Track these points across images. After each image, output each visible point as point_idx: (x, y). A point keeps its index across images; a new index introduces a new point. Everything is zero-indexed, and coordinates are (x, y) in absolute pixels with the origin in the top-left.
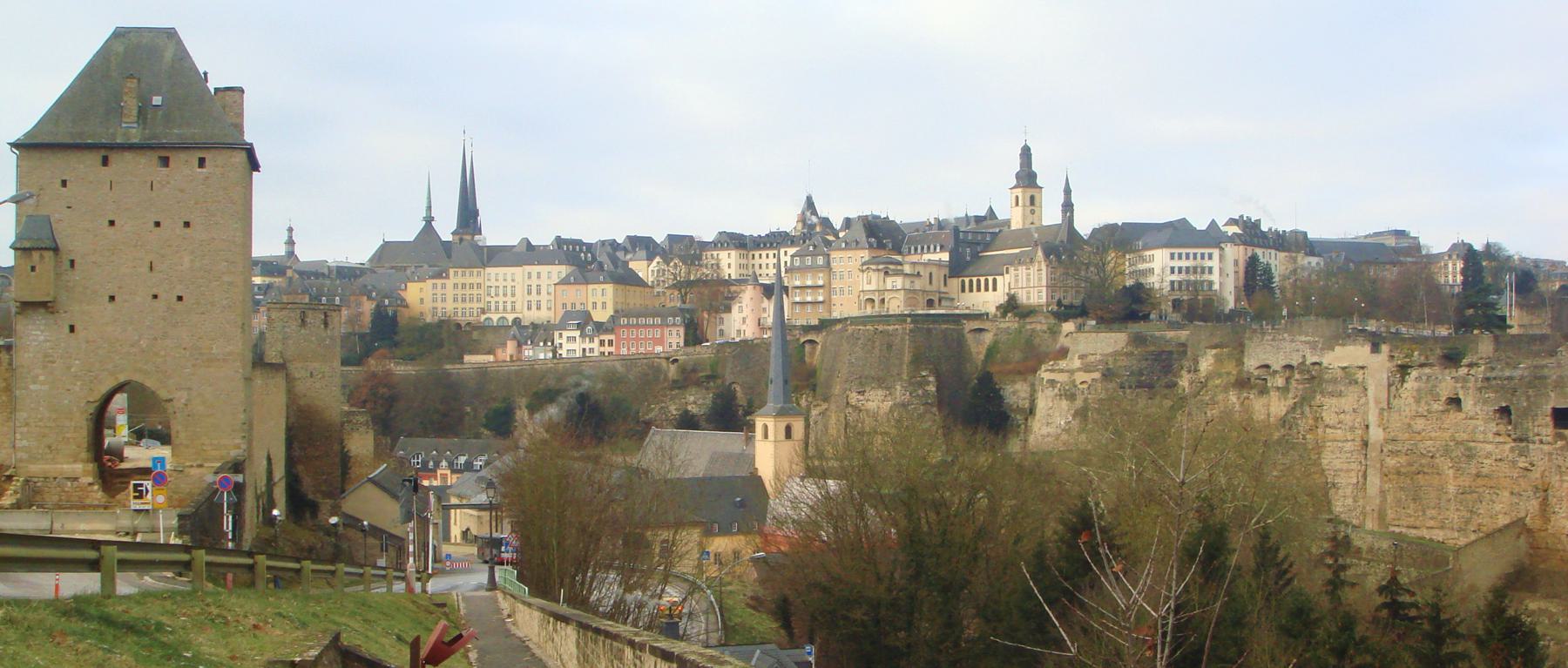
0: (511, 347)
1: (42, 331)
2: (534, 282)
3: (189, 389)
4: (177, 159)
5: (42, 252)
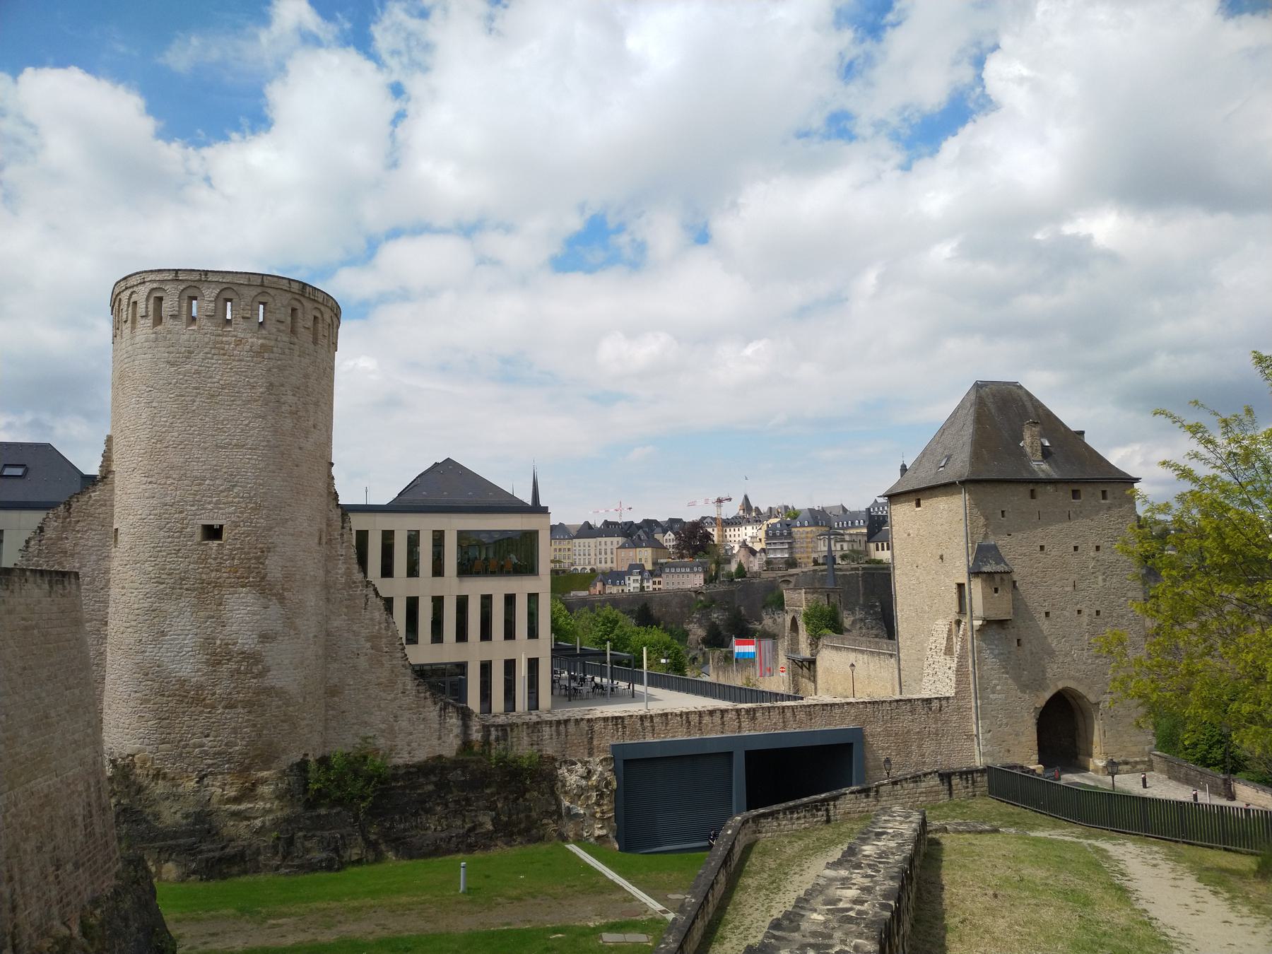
0: (599, 586)
4: (1085, 491)
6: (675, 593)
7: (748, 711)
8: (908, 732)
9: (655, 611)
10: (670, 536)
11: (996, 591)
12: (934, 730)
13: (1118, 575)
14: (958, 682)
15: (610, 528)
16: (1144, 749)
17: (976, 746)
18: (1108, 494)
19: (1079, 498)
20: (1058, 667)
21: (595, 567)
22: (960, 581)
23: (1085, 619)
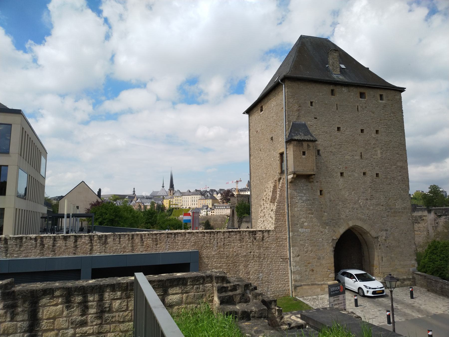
1: (305, 194)
2: (193, 199)
3: (387, 230)
5: (308, 143)
6: (219, 216)
7: (100, 237)
8: (237, 255)
9: (212, 223)
10: (219, 195)
11: (304, 153)
12: (258, 255)
13: (391, 150)
14: (277, 220)
15: (198, 192)
16: (409, 270)
17: (289, 267)
18: (384, 97)
19: (365, 98)
20: (350, 211)
21: (190, 207)
22: (281, 151)
23: (368, 179)
